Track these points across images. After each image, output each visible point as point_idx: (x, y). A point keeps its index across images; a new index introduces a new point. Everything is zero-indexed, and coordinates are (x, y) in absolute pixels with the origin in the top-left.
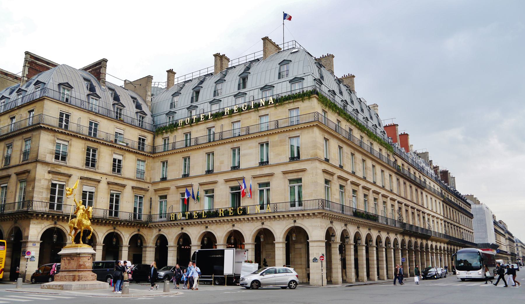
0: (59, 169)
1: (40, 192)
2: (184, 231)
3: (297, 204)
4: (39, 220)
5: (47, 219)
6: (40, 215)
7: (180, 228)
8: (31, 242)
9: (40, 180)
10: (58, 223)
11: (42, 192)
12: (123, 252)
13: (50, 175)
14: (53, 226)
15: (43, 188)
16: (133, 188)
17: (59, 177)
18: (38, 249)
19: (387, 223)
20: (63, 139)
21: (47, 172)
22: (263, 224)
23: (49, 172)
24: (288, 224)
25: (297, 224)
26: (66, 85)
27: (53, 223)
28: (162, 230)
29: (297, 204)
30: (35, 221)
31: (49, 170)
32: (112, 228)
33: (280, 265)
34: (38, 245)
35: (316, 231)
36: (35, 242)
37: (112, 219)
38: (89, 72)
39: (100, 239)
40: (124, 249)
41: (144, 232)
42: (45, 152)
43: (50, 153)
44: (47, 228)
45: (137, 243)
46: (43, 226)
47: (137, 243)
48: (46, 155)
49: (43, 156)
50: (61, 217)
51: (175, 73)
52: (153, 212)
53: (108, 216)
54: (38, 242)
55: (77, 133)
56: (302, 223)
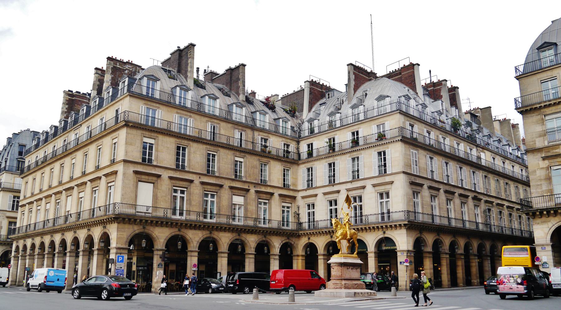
0: (557, 151)
1: (538, 185)
2: (310, 241)
3: (178, 212)
4: (544, 219)
6: (538, 213)
8: (538, 245)
9: (535, 171)
11: (541, 184)
15: (541, 180)
16: (280, 195)
18: (550, 253)
20: (553, 111)
21: (541, 159)
22: (384, 233)
23: (544, 159)
24: (379, 235)
25: (386, 235)
26: (545, 45)
28: (311, 238)
29: (178, 212)
30: (538, 220)
31: (543, 155)
32: (237, 234)
35: (403, 241)
36: (543, 245)
37: (360, 223)
38: (302, 90)
41: (293, 241)
42: (533, 138)
43: (540, 136)
44: (556, 226)
45: (262, 251)
46: (550, 225)
47: (262, 251)
49: (531, 143)
51: (255, 93)
52: (302, 220)
53: (380, 220)
54: (547, 245)
55: (540, 103)
56: (390, 234)
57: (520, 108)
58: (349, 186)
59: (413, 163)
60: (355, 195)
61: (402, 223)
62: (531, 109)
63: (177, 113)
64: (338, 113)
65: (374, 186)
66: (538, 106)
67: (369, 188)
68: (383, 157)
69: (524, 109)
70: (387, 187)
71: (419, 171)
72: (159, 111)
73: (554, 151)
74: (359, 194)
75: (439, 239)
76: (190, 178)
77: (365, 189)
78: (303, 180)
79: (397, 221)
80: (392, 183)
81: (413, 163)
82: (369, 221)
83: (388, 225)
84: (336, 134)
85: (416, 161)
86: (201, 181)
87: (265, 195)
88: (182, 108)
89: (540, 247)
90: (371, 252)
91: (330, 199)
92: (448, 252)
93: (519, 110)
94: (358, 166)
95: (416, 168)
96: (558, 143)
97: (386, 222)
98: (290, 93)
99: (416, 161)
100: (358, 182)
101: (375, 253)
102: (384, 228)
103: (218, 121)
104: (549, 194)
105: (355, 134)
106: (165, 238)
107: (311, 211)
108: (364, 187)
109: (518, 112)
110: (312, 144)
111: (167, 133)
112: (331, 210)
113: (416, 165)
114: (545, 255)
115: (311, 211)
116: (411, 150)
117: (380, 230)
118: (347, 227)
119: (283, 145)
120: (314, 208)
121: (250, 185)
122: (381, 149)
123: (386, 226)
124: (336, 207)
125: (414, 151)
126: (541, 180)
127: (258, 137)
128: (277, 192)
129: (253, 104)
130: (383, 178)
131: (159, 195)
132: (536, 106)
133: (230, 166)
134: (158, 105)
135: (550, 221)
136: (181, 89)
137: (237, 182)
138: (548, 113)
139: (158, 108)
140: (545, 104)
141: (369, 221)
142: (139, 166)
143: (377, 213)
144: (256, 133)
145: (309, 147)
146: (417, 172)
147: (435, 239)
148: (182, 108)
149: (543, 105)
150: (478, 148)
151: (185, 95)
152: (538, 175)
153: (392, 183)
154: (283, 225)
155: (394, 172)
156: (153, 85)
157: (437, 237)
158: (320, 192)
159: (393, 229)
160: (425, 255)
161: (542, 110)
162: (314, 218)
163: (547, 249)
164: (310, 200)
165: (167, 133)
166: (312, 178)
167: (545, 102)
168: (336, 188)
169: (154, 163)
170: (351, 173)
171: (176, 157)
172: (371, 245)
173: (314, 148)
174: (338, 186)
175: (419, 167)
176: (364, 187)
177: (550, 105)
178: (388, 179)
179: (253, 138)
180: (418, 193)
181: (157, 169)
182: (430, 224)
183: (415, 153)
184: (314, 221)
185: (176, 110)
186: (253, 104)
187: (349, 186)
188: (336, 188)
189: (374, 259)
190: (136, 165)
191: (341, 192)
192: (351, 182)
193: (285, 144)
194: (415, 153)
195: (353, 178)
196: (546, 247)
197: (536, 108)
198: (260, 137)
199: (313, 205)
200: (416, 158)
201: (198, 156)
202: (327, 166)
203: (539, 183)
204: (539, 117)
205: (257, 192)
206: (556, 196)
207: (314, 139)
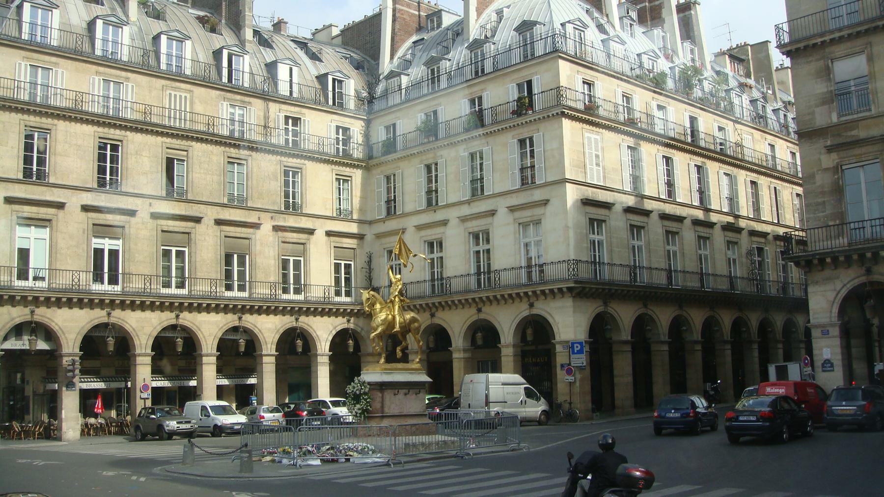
0: (854, 133)
2: (437, 321)
4: (827, 272)
5: (848, 262)
7: (473, 310)
8: (816, 327)
10: (875, 269)
12: (204, 367)
13: (834, 155)
14: (863, 279)
17: (857, 151)
19: (671, 192)
21: (824, 151)
23: (830, 150)
24: (522, 310)
27: (863, 271)
31: (829, 143)
33: (212, 399)
34: (835, 331)
39: (323, 344)
40: (265, 359)
43: (824, 103)
44: (849, 286)
46: (838, 285)
48: (813, 113)
50: (869, 255)
54: (832, 325)
55: (822, 35)
56: (544, 308)
57: (785, 45)
58: (466, 210)
59: (591, 161)
60: (476, 229)
61: (563, 286)
62: (806, 47)
63: (97, 73)
64: (446, 59)
65: (512, 209)
66: (819, 40)
67: (502, 213)
68: (528, 149)
69: (793, 47)
70: (538, 211)
71: (604, 177)
72: (57, 72)
73: (849, 133)
74: (484, 228)
75: (646, 314)
76: (130, 207)
77: (495, 217)
78: (379, 201)
79: (554, 281)
80: (546, 202)
81: (591, 161)
82: (502, 283)
83: (539, 289)
84: (439, 104)
85: (597, 156)
86: (152, 211)
87: (295, 235)
88: (109, 62)
89: (819, 330)
90: (507, 346)
91: (429, 238)
92: (667, 339)
93: (784, 50)
94: (481, 170)
95: (598, 171)
96: (855, 116)
97: (536, 285)
98: (357, 20)
99: (597, 156)
100: (482, 202)
101: (514, 346)
102: (531, 298)
103: (188, 87)
104: (838, 222)
105: (476, 101)
106: (77, 330)
107: (435, 255)
108: (492, 213)
109: (783, 54)
110: (394, 125)
111: (74, 115)
112: (433, 259)
113: (598, 165)
114: (828, 347)
115: (482, 247)
116: (587, 135)
117: (525, 300)
118: (397, 307)
119: (334, 130)
120: (441, 251)
121: (262, 215)
122: (525, 133)
123: (534, 292)
124: (440, 255)
125: (593, 136)
126: (823, 193)
127: (278, 112)
128: (321, 227)
129: (271, 47)
130: (529, 192)
131: (62, 244)
132: (814, 41)
133: (216, 178)
134: (54, 59)
135: (838, 278)
136: (107, 23)
137: (232, 210)
138: (838, 54)
139: (56, 64)
140: (832, 36)
141: (502, 283)
142: (17, 186)
143: (518, 265)
144: (273, 107)
145: (388, 132)
146: (598, 180)
147: (637, 314)
148: (109, 62)
149: (827, 38)
150: (738, 126)
151: (115, 34)
152: (818, 184)
153: (546, 202)
154: (338, 293)
155: (550, 179)
156: (44, 18)
157: (643, 310)
158: (453, 214)
159: (548, 298)
160: (615, 348)
161: (827, 50)
162: (489, 265)
163: (831, 334)
164: (432, 234)
165: (74, 115)
166: (395, 196)
167: (832, 32)
168: (439, 216)
169: (52, 180)
170: (517, 172)
171: (96, 164)
172: (506, 330)
173: (398, 133)
174: (444, 211)
175: (604, 168)
176: (492, 213)
177: (841, 39)
178: (538, 195)
179: (266, 118)
180: (600, 222)
181: (55, 190)
182: (626, 286)
183: (596, 140)
184: (489, 272)
185: (94, 68)
186: (271, 47)
187: (466, 210)
188: (439, 216)
189: (511, 359)
190: (10, 185)
191: (450, 224)
192: (468, 202)
193: (338, 128)
194: (596, 140)
195: (473, 195)
196: (831, 329)
197: (815, 45)
198: (282, 116)
199: (440, 244)
200: (597, 150)
201: (146, 159)
202: (424, 172)
203: (820, 200)
204: (821, 63)
205: (276, 229)
206: (852, 225)
207: (398, 114)
